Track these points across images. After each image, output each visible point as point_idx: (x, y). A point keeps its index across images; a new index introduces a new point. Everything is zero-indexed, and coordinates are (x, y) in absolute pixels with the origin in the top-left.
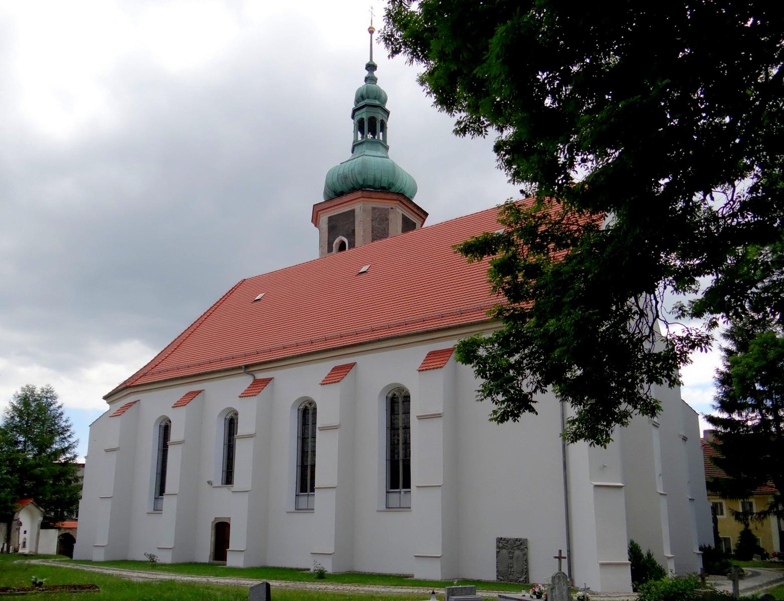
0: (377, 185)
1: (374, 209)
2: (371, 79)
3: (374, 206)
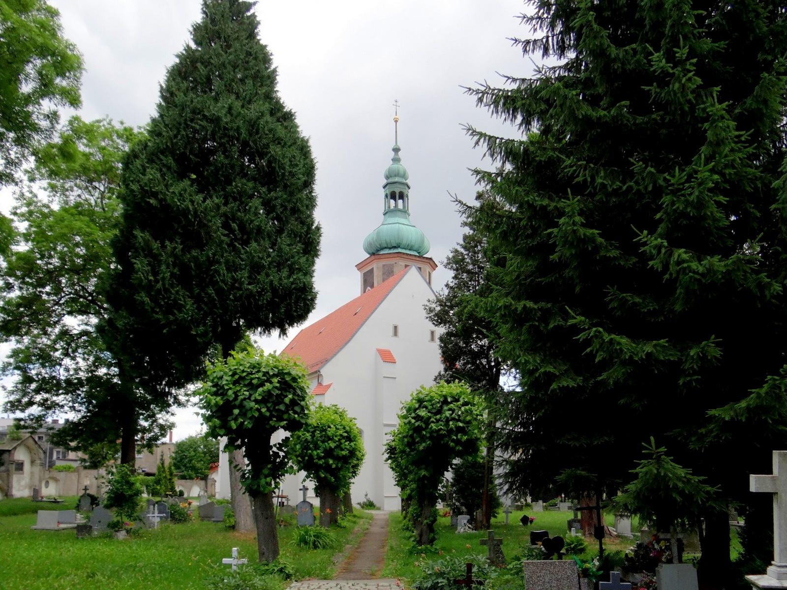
0: (389, 246)
2: (396, 160)
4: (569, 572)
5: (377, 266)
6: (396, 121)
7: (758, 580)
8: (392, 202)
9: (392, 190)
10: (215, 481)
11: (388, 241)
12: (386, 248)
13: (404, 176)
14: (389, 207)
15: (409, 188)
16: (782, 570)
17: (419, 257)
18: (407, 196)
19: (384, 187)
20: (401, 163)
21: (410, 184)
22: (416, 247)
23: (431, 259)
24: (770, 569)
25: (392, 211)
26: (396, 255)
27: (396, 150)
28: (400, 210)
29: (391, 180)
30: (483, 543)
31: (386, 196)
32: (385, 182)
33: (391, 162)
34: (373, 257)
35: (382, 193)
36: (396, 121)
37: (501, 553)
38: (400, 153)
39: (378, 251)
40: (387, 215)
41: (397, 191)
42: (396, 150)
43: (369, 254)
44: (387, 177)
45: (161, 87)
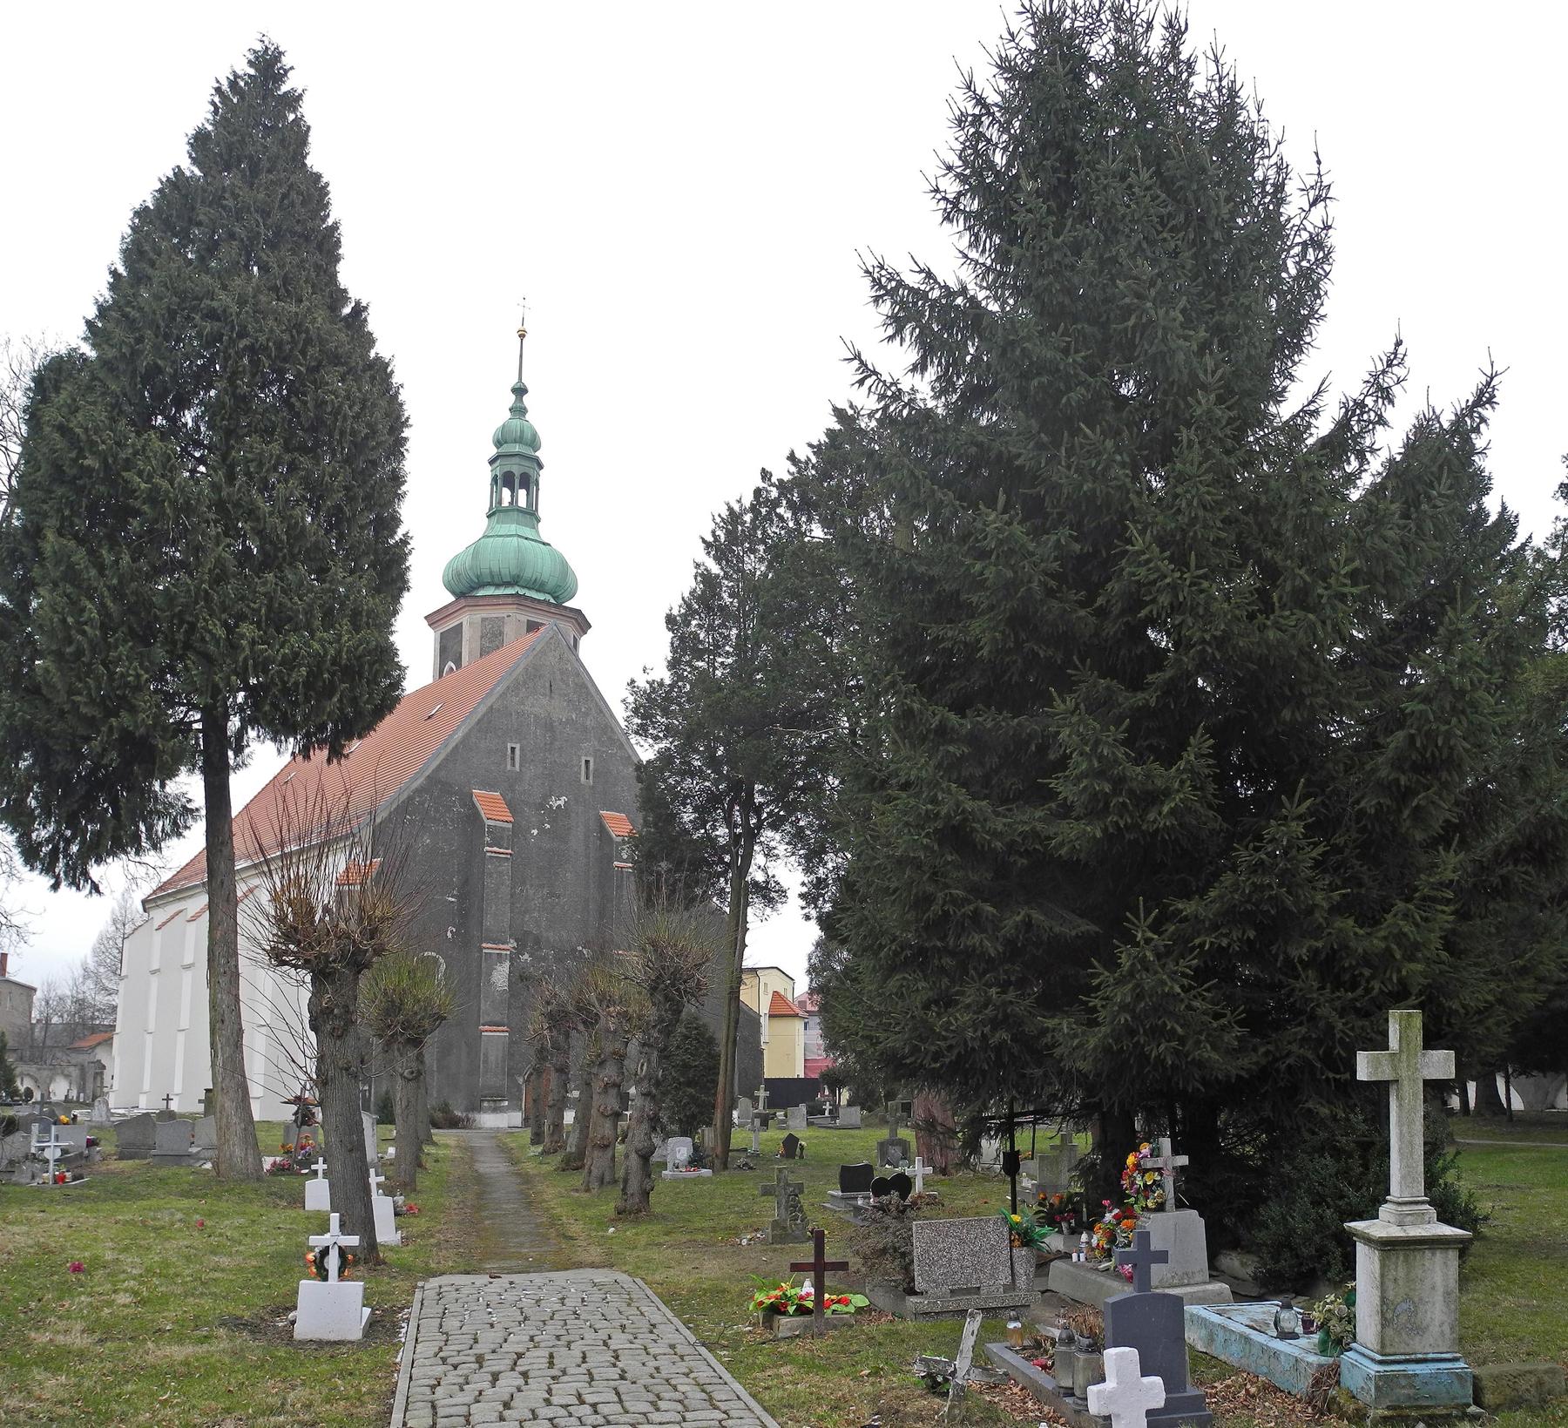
0: (496, 580)
1: (483, 620)
2: (519, 411)
3: (485, 616)
4: (993, 1238)
5: (469, 621)
6: (522, 336)
7: (1367, 1227)
8: (506, 493)
9: (506, 469)
10: (104, 1067)
11: (495, 569)
12: (489, 584)
13: (534, 443)
14: (500, 502)
15: (541, 466)
16: (1405, 1208)
17: (556, 606)
18: (537, 485)
19: (492, 462)
20: (528, 417)
21: (543, 460)
22: (551, 584)
23: (579, 612)
24: (1384, 1210)
25: (506, 510)
26: (510, 600)
27: (520, 391)
28: (520, 510)
29: (506, 449)
30: (767, 1192)
31: (495, 479)
32: (493, 451)
33: (508, 415)
34: (463, 602)
35: (486, 474)
36: (522, 336)
37: (801, 1210)
38: (525, 398)
39: (473, 589)
40: (495, 518)
41: (517, 471)
42: (520, 391)
43: (453, 593)
44: (498, 443)
45: (114, 273)
